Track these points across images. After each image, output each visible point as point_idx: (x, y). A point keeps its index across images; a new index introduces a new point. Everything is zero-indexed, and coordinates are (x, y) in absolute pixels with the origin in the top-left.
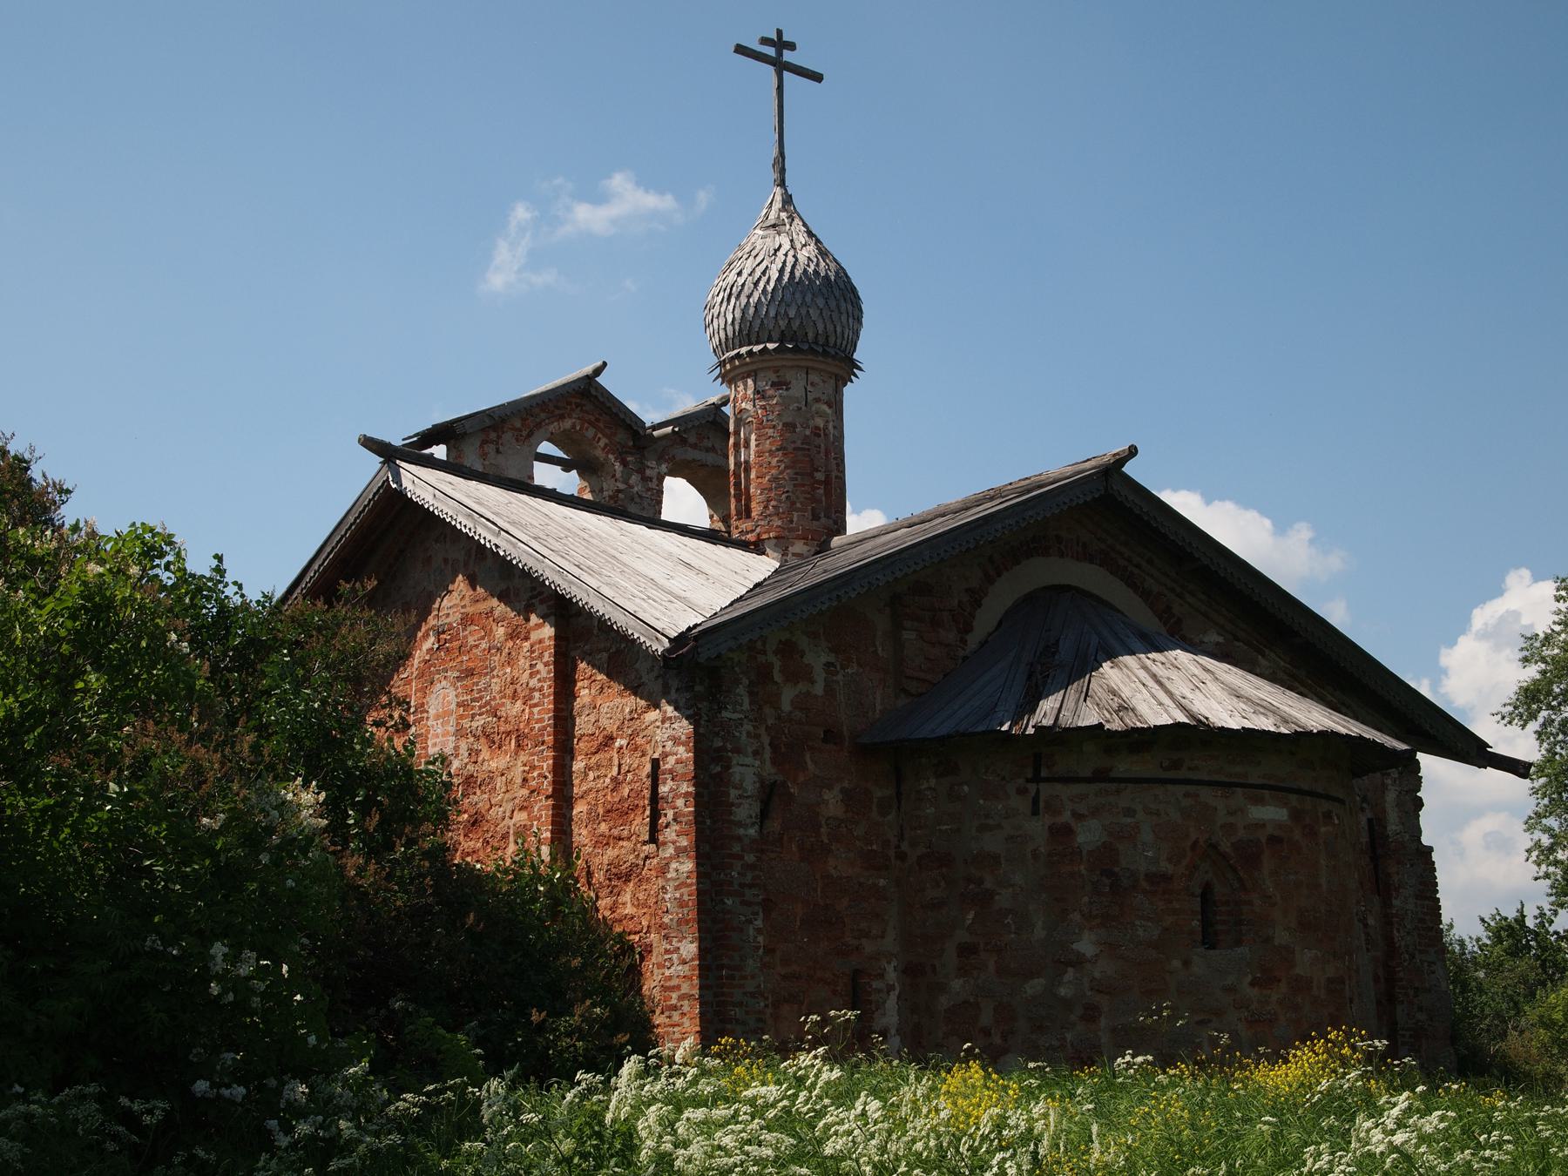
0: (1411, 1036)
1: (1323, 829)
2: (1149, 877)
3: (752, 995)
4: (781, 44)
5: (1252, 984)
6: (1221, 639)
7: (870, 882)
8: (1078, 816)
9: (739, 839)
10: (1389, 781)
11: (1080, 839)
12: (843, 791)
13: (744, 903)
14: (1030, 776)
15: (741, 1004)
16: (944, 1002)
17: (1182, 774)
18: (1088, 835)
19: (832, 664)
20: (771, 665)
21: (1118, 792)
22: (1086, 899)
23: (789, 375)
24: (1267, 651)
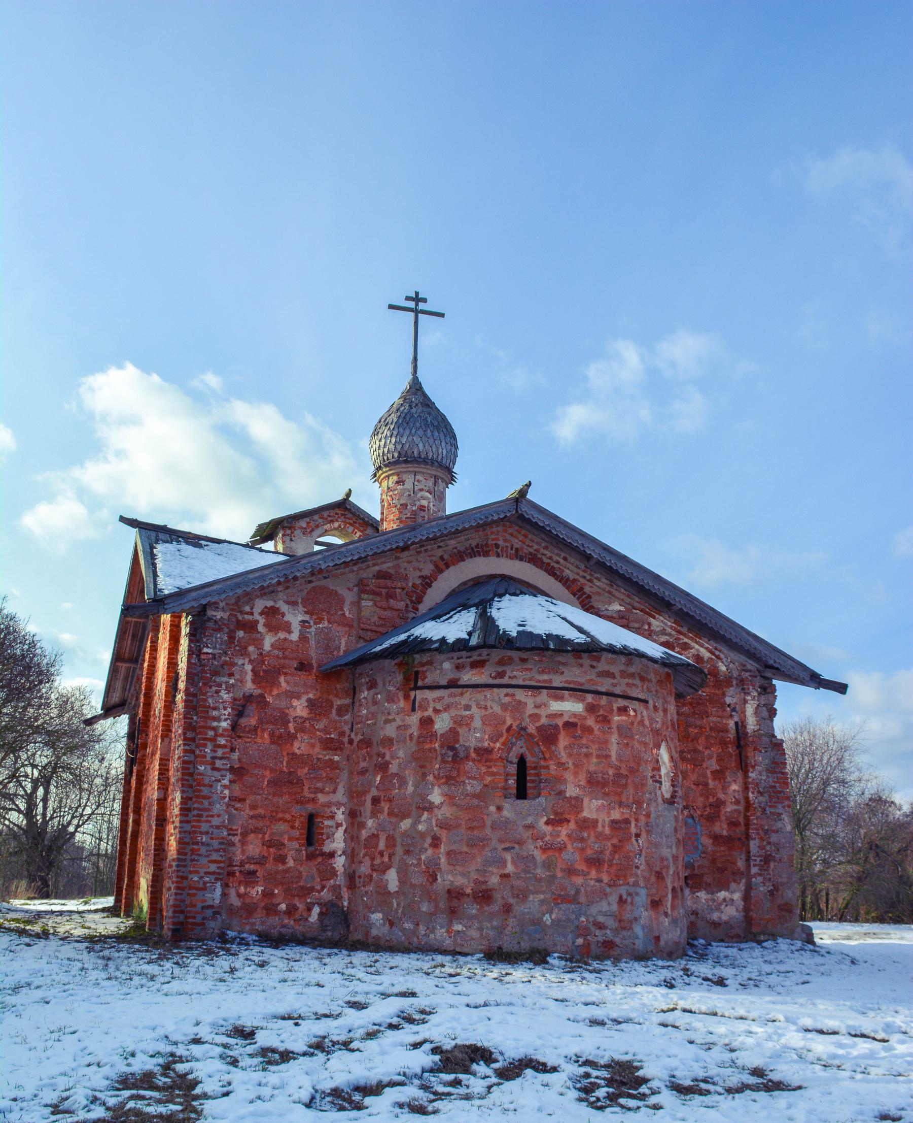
0: (761, 861)
1: (616, 718)
2: (477, 750)
3: (218, 827)
4: (417, 299)
5: (547, 823)
6: (622, 609)
7: (327, 758)
8: (436, 711)
9: (214, 729)
10: (749, 698)
11: (437, 727)
12: (309, 700)
13: (214, 769)
14: (412, 686)
15: (207, 833)
16: (364, 834)
17: (505, 680)
18: (442, 724)
19: (307, 622)
20: (257, 622)
21: (462, 694)
22: (437, 766)
23: (405, 477)
24: (657, 616)
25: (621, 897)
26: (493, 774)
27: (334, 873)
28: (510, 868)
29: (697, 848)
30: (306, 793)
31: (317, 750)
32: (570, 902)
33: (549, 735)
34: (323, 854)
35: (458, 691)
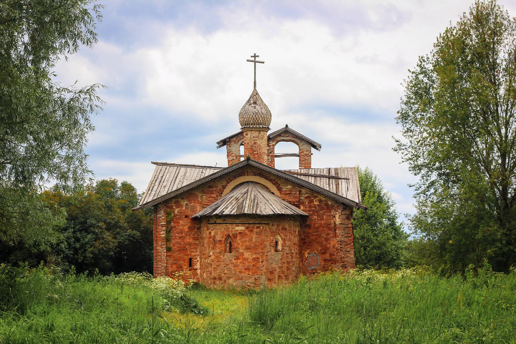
2: (219, 241)
4: (255, 56)
25: (255, 278)
26: (222, 247)
27: (197, 274)
28: (226, 272)
29: (318, 264)
30: (188, 253)
31: (191, 240)
32: (240, 280)
33: (235, 236)
34: (194, 269)
35: (215, 225)
